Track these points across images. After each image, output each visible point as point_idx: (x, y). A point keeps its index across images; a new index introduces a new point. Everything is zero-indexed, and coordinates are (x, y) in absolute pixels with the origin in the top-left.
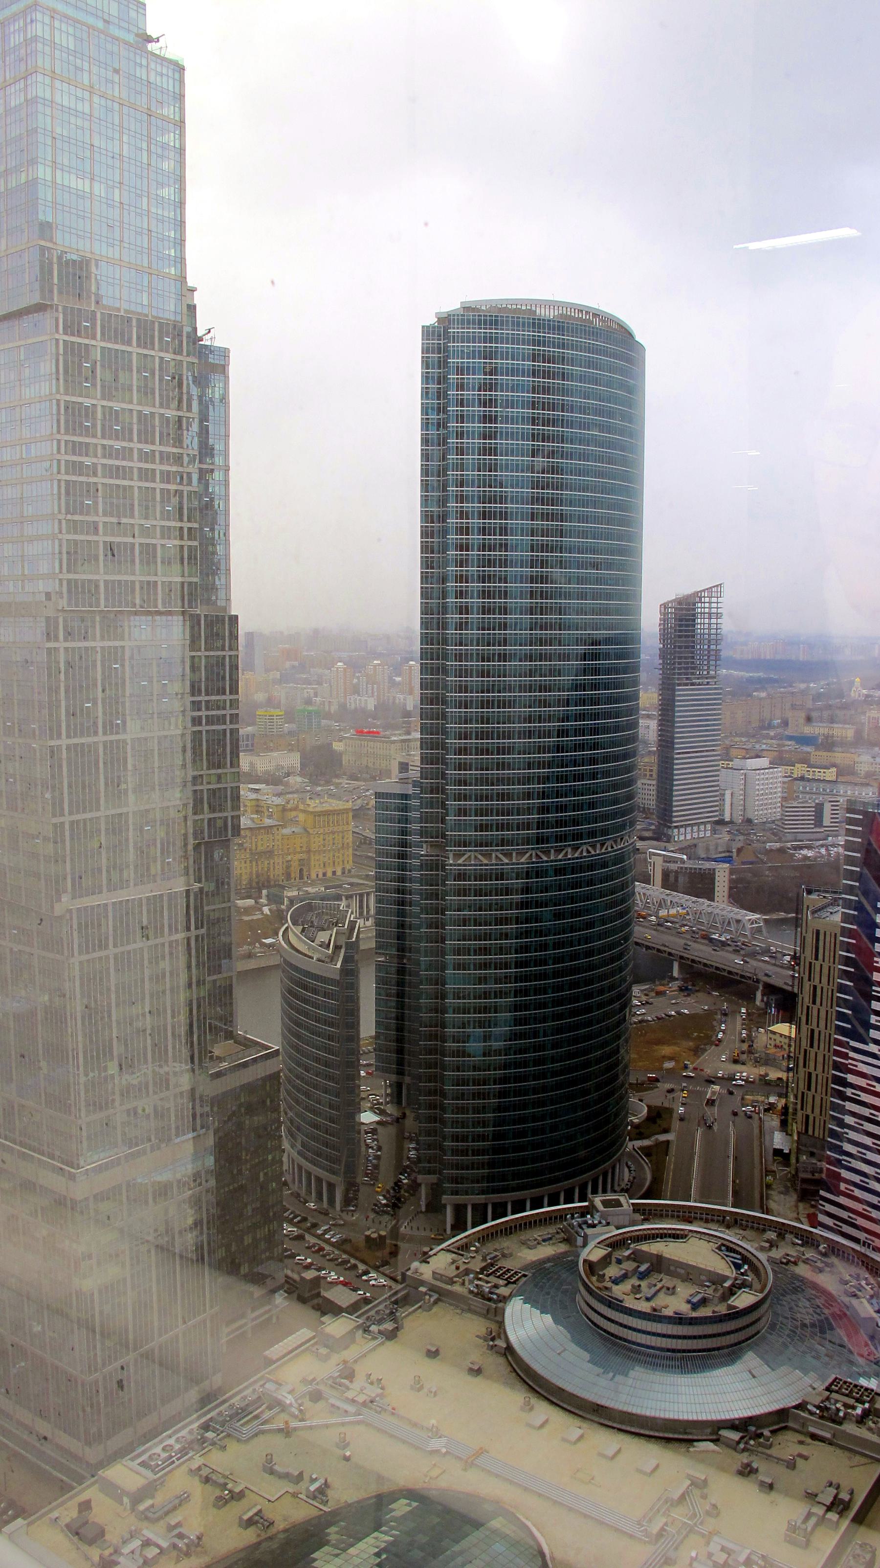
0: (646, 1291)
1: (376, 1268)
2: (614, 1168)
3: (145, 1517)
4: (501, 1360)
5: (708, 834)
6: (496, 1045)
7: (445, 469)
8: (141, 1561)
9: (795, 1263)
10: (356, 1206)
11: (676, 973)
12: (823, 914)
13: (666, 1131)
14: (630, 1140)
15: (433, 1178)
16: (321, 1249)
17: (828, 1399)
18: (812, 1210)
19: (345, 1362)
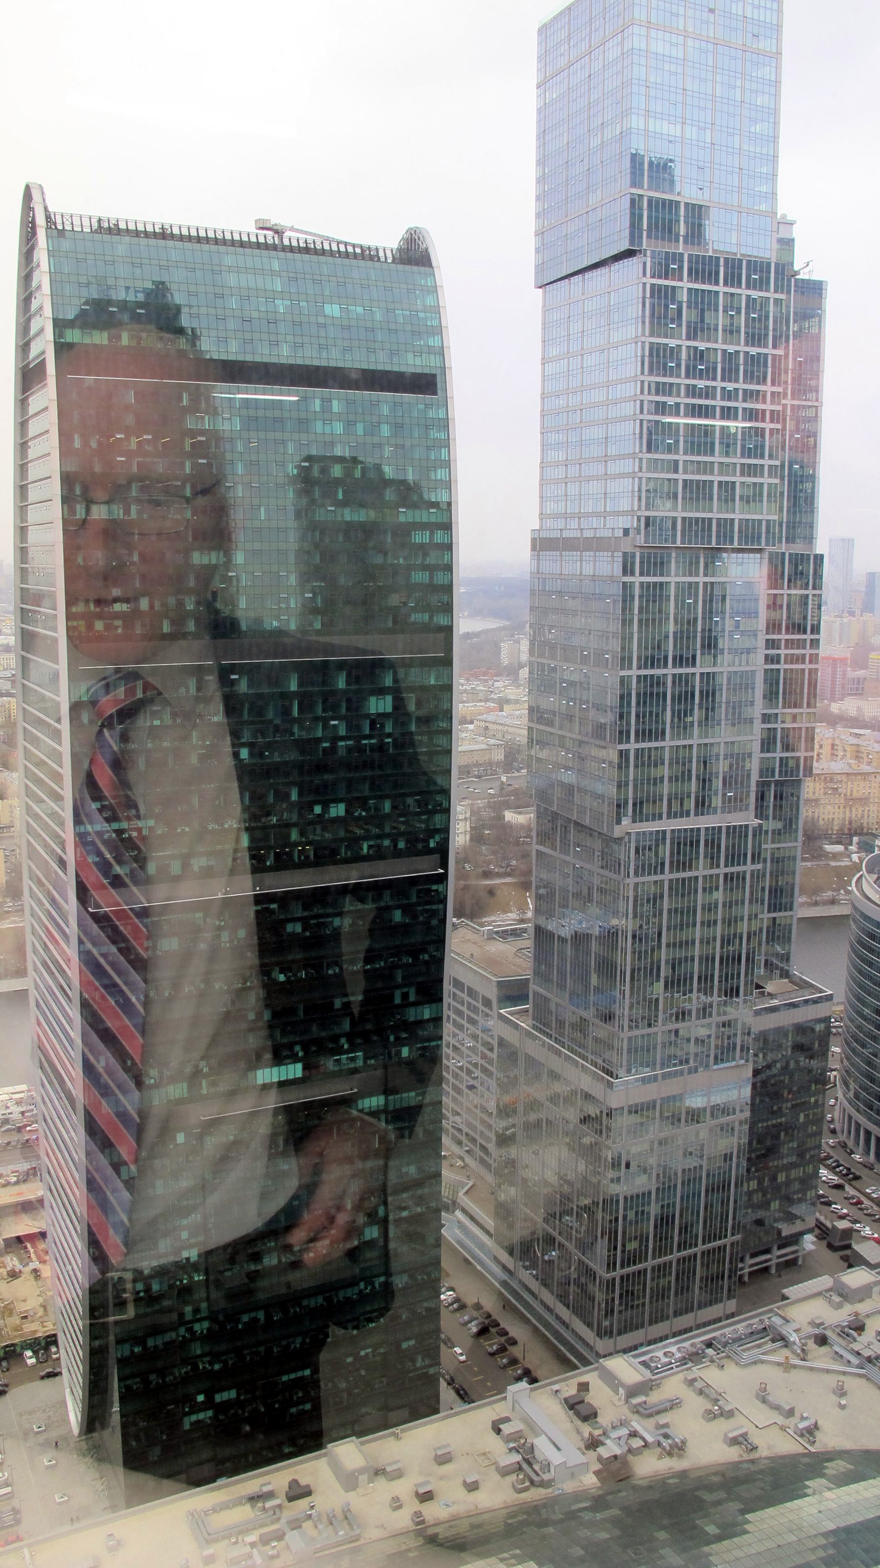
3: (636, 1410)
8: (626, 1448)
16: (859, 1202)
19: (857, 1314)
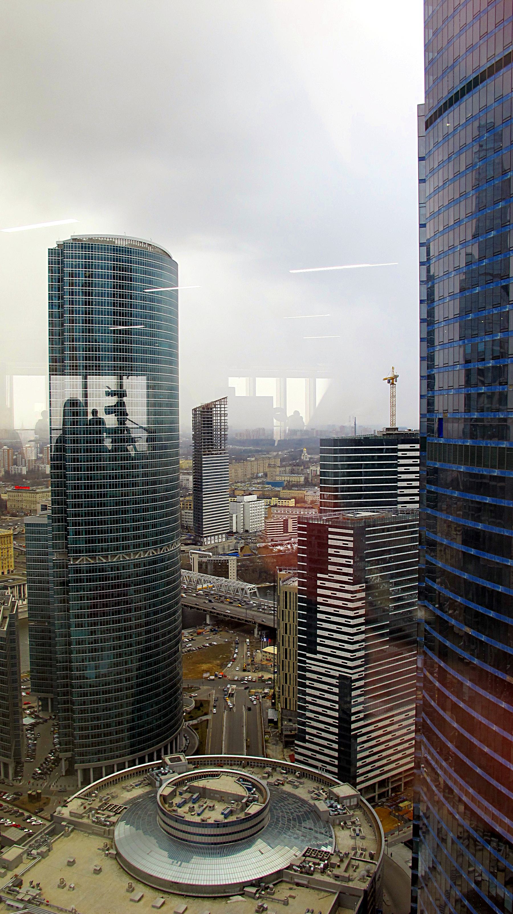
0: (197, 810)
1: (36, 814)
2: (176, 739)
4: (114, 862)
5: (224, 540)
6: (103, 671)
7: (63, 332)
9: (283, 784)
10: (22, 776)
11: (208, 622)
12: (288, 582)
13: (206, 714)
14: (185, 721)
15: (69, 754)
17: (304, 861)
18: (292, 753)
19: (16, 876)
